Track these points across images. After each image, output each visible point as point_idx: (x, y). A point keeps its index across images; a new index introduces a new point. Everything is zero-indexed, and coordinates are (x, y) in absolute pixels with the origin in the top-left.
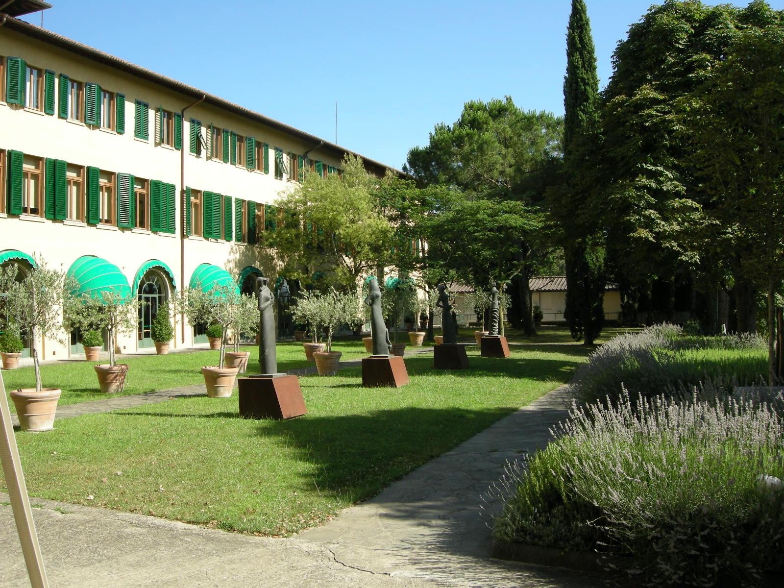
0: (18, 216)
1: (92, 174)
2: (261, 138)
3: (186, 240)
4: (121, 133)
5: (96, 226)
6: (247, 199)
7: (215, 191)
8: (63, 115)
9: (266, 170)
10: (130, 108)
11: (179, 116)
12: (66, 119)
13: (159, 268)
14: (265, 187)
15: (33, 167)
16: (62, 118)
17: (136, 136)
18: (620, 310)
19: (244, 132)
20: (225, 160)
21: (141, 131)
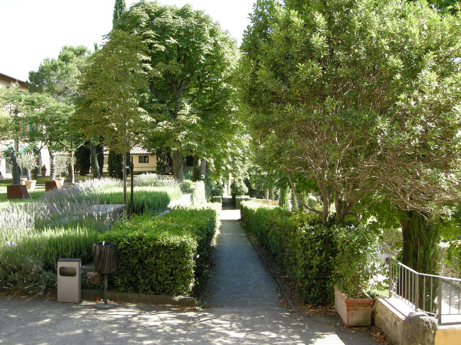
18: (157, 165)
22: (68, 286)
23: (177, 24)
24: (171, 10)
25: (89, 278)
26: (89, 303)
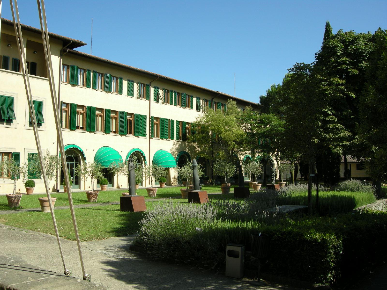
0: (74, 130)
1: (107, 112)
2: (189, 93)
3: (151, 140)
4: (121, 94)
5: (109, 134)
6: (182, 121)
7: (166, 117)
8: (94, 88)
9: (192, 108)
10: (125, 84)
11: (148, 85)
12: (96, 89)
13: (138, 152)
14: (191, 115)
15: (82, 110)
16: (94, 89)
17: (128, 95)
19: (179, 91)
20: (171, 104)
21: (130, 93)
22: (233, 264)
23: (367, 49)
24: (364, 38)
25: (252, 260)
26: (248, 280)
